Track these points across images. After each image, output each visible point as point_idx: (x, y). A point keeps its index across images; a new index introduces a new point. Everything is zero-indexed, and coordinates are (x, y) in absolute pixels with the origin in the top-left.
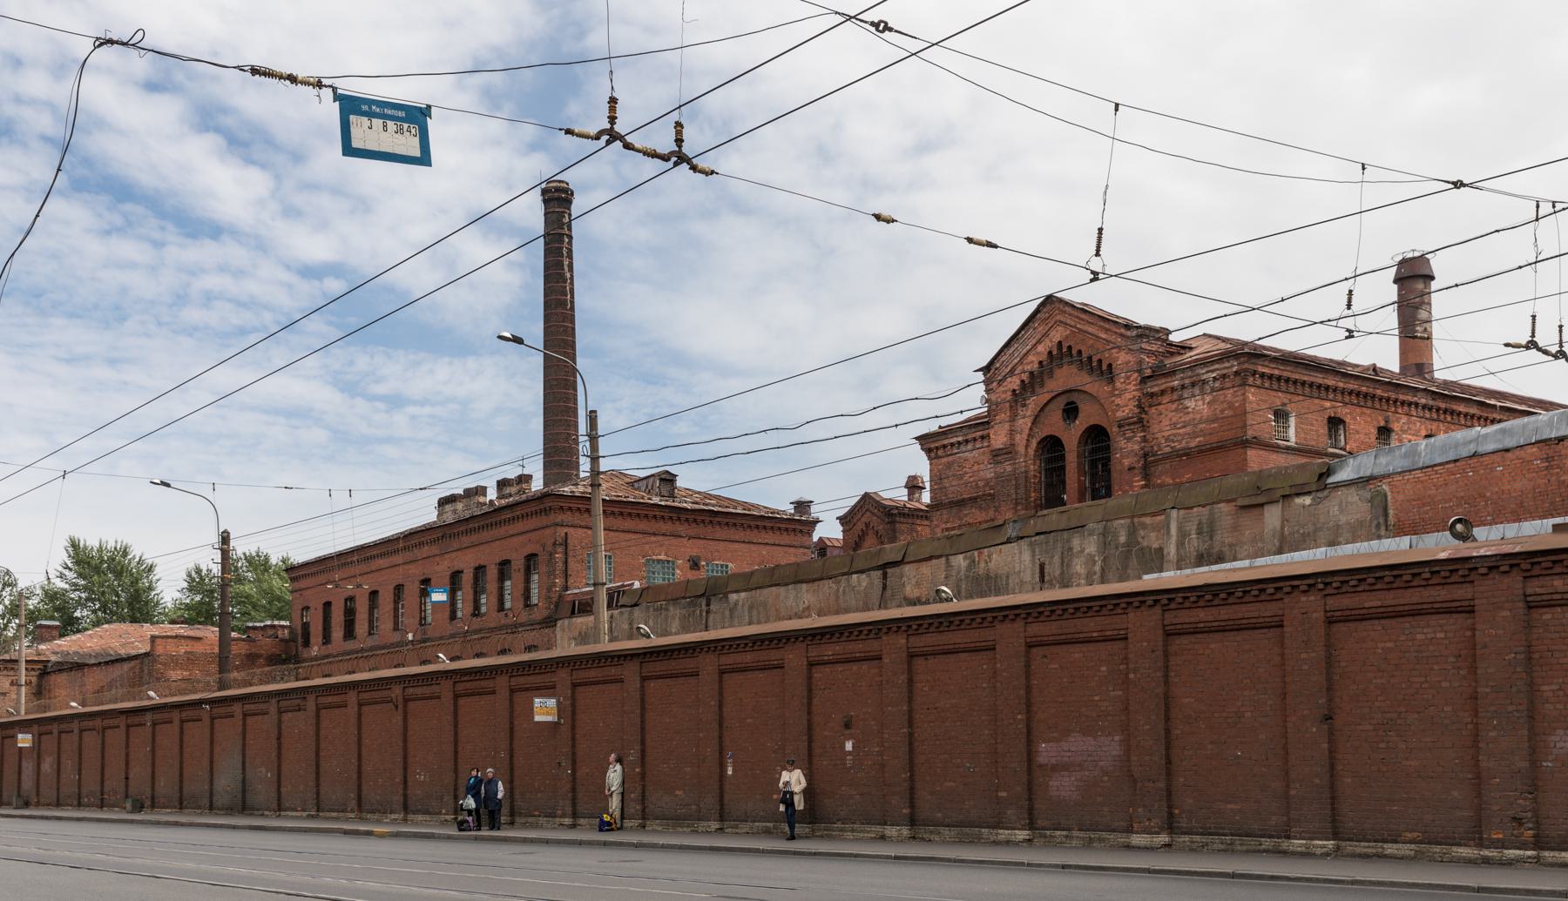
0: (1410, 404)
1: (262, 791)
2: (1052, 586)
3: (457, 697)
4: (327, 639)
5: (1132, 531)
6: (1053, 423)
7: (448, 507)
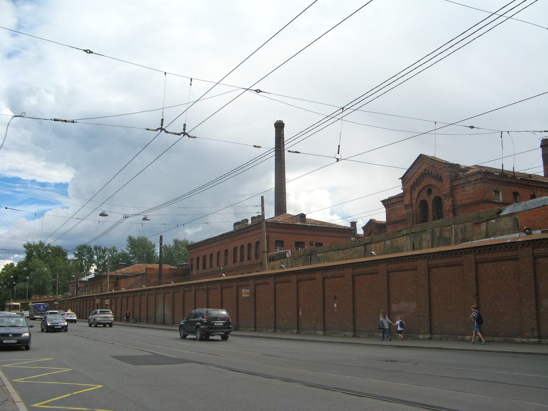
0: (541, 187)
1: (168, 319)
2: (416, 250)
3: (222, 289)
4: (198, 269)
5: (441, 232)
6: (424, 196)
7: (237, 226)
